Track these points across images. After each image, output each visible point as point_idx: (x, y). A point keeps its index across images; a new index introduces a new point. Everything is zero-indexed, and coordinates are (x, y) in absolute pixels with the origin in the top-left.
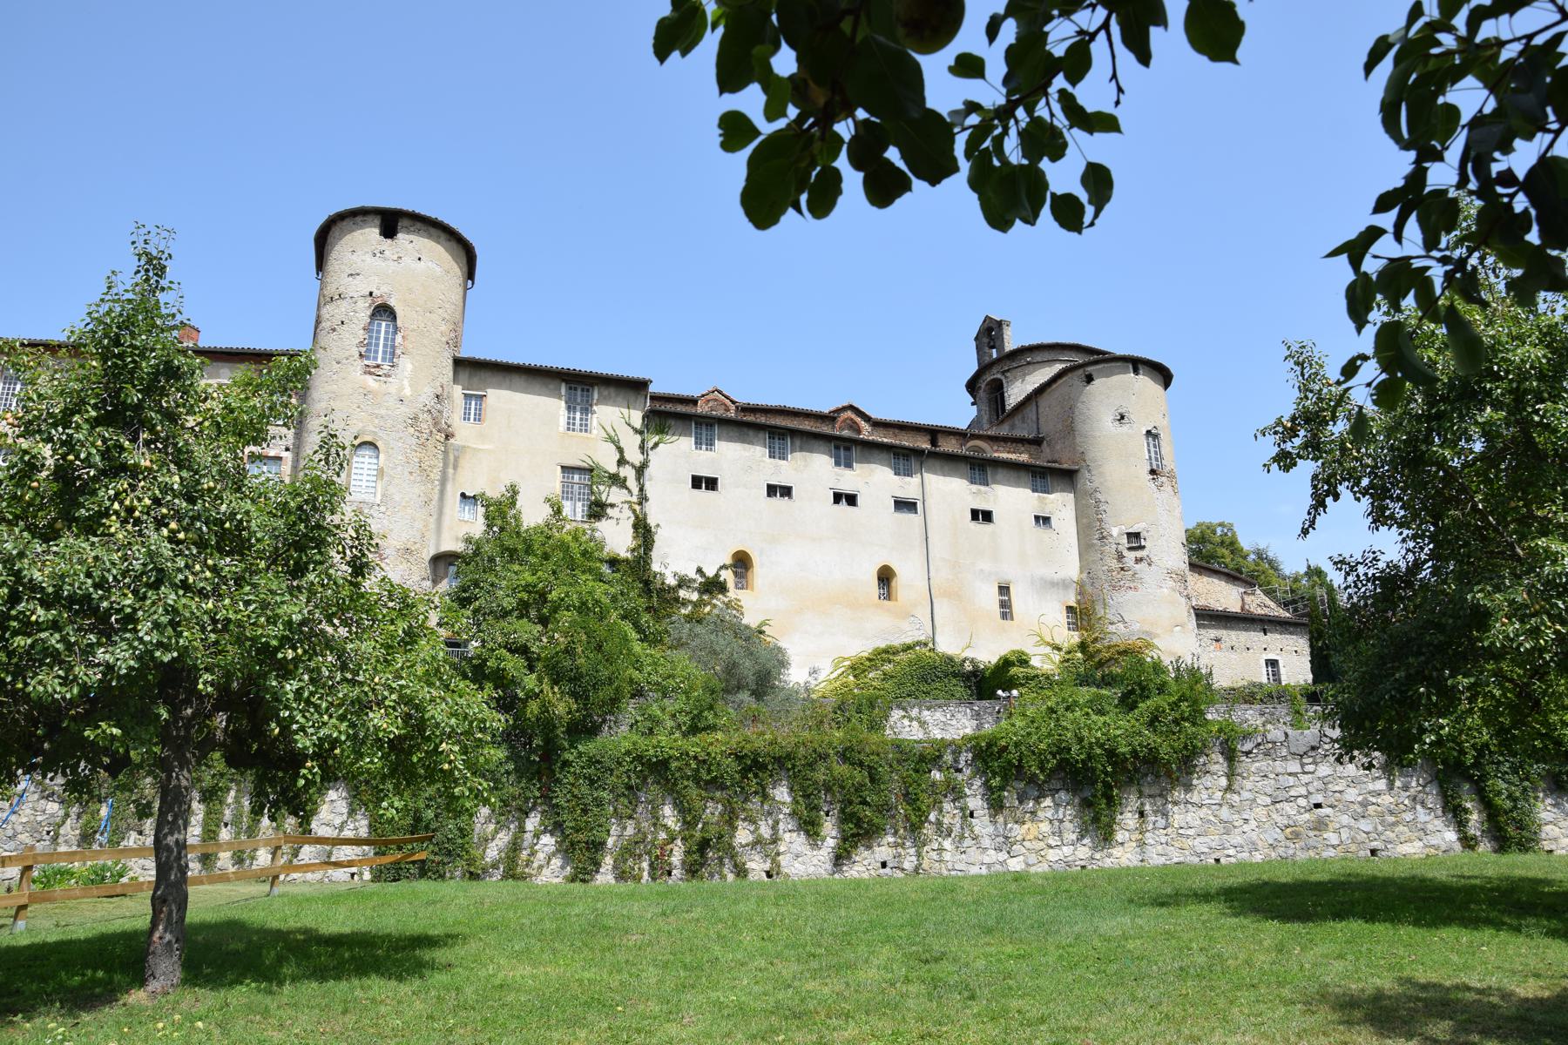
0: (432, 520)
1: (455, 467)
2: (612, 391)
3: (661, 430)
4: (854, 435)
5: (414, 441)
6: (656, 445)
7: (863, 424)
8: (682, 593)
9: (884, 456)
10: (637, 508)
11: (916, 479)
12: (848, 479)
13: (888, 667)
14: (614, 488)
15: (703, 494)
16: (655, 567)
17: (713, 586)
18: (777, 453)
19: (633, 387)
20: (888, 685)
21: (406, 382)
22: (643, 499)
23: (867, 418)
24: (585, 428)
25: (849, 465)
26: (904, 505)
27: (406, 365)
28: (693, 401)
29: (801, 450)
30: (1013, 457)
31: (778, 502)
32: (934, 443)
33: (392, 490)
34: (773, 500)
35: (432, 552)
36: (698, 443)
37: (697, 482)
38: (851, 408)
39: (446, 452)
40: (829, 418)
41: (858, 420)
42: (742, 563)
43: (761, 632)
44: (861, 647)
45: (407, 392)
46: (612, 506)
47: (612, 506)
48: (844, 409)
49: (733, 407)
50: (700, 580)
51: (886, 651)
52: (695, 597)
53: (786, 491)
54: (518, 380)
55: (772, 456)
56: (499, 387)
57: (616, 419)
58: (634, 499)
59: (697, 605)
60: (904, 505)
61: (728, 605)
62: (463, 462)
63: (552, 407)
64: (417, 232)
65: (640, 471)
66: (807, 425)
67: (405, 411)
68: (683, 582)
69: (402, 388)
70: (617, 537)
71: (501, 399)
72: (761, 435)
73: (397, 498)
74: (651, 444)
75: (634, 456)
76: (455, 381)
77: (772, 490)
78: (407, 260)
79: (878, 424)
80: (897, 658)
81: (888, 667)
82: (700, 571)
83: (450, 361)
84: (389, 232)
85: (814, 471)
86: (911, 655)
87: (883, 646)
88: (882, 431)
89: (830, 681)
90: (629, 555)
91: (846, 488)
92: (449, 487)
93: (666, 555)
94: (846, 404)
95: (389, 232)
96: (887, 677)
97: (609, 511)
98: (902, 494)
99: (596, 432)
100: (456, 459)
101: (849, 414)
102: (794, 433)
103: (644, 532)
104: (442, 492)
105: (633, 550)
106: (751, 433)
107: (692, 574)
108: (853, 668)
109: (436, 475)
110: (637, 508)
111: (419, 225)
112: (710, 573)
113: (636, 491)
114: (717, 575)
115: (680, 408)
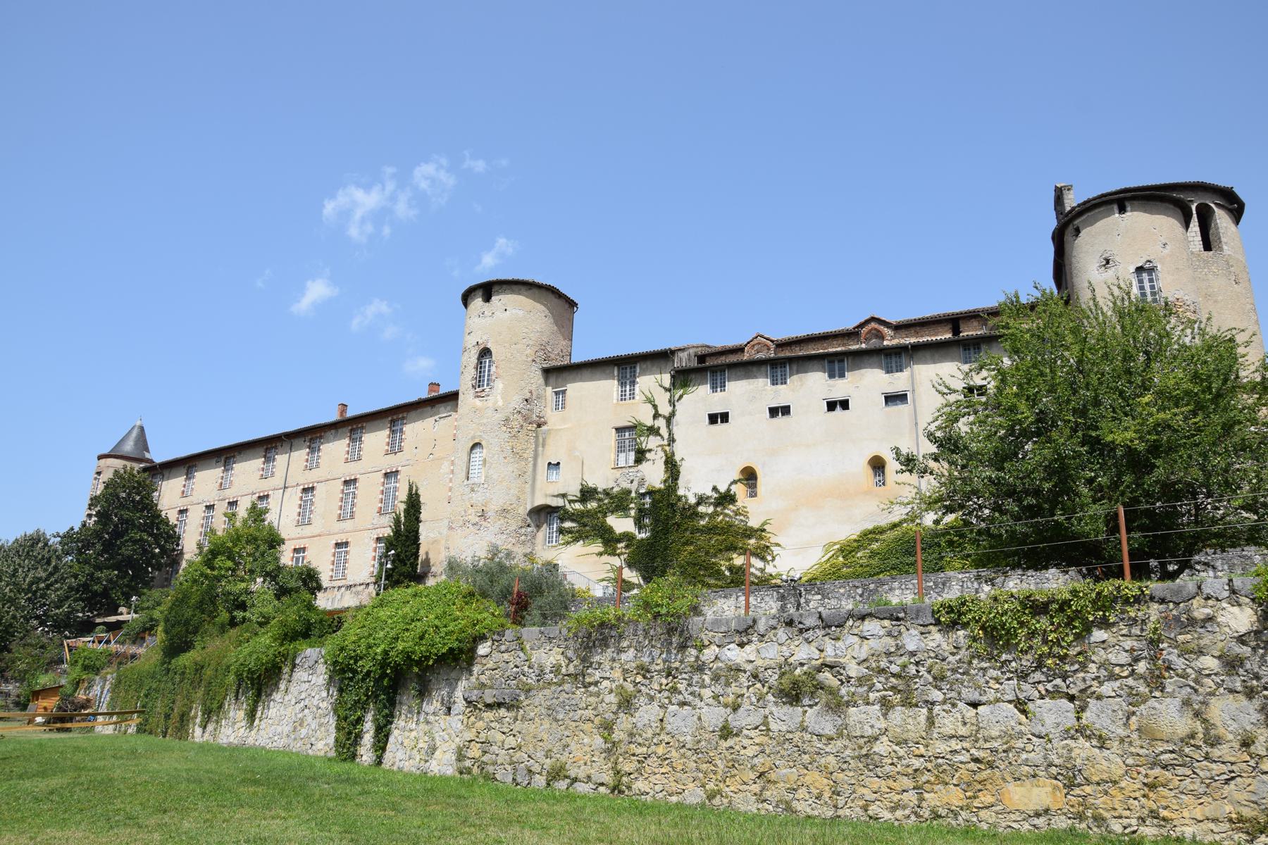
0: (528, 486)
1: (543, 446)
2: (649, 363)
3: (685, 385)
5: (507, 435)
6: (681, 397)
7: (885, 330)
8: (701, 509)
9: (875, 359)
10: (667, 448)
11: (906, 373)
12: (840, 388)
13: (875, 546)
14: (651, 437)
15: (720, 427)
16: (681, 492)
17: (726, 499)
18: (718, 386)
19: (660, 358)
20: (875, 562)
21: (499, 397)
22: (672, 440)
24: (632, 396)
25: (842, 375)
26: (894, 399)
27: (499, 385)
28: (740, 350)
29: (798, 372)
30: (913, 340)
31: (780, 420)
32: (956, 331)
33: (491, 472)
34: (714, 427)
35: (529, 508)
36: (714, 388)
37: (713, 419)
38: (873, 319)
39: (537, 437)
40: (852, 335)
41: (881, 328)
42: (749, 476)
43: (764, 530)
44: (848, 531)
45: (500, 403)
46: (650, 451)
47: (650, 451)
49: (773, 346)
50: (716, 495)
51: (871, 532)
52: (711, 510)
53: (786, 410)
54: (586, 373)
55: (774, 383)
56: (574, 381)
57: (652, 383)
58: (666, 442)
59: (712, 516)
60: (894, 399)
61: (737, 513)
62: (549, 441)
63: (609, 386)
64: (504, 292)
65: (669, 420)
67: (500, 416)
68: (701, 500)
69: (496, 402)
70: (654, 474)
71: (577, 389)
72: (763, 368)
73: (495, 477)
74: (677, 397)
75: (665, 409)
76: (547, 384)
77: (774, 412)
78: (498, 314)
80: (884, 537)
81: (875, 546)
82: (715, 489)
83: (539, 373)
84: (487, 299)
85: (812, 386)
86: (896, 533)
87: (870, 527)
88: (903, 333)
89: (821, 564)
90: (662, 486)
91: (838, 396)
92: (539, 460)
93: (688, 482)
94: (867, 317)
95: (487, 299)
96: (873, 554)
97: (648, 455)
98: (891, 390)
99: (639, 397)
100: (544, 440)
101: (873, 325)
102: (791, 360)
103: (672, 467)
104: (535, 465)
105: (665, 481)
106: (755, 369)
107: (709, 493)
108: (841, 550)
109: (529, 454)
110: (667, 448)
112: (723, 489)
113: (666, 436)
114: (729, 490)
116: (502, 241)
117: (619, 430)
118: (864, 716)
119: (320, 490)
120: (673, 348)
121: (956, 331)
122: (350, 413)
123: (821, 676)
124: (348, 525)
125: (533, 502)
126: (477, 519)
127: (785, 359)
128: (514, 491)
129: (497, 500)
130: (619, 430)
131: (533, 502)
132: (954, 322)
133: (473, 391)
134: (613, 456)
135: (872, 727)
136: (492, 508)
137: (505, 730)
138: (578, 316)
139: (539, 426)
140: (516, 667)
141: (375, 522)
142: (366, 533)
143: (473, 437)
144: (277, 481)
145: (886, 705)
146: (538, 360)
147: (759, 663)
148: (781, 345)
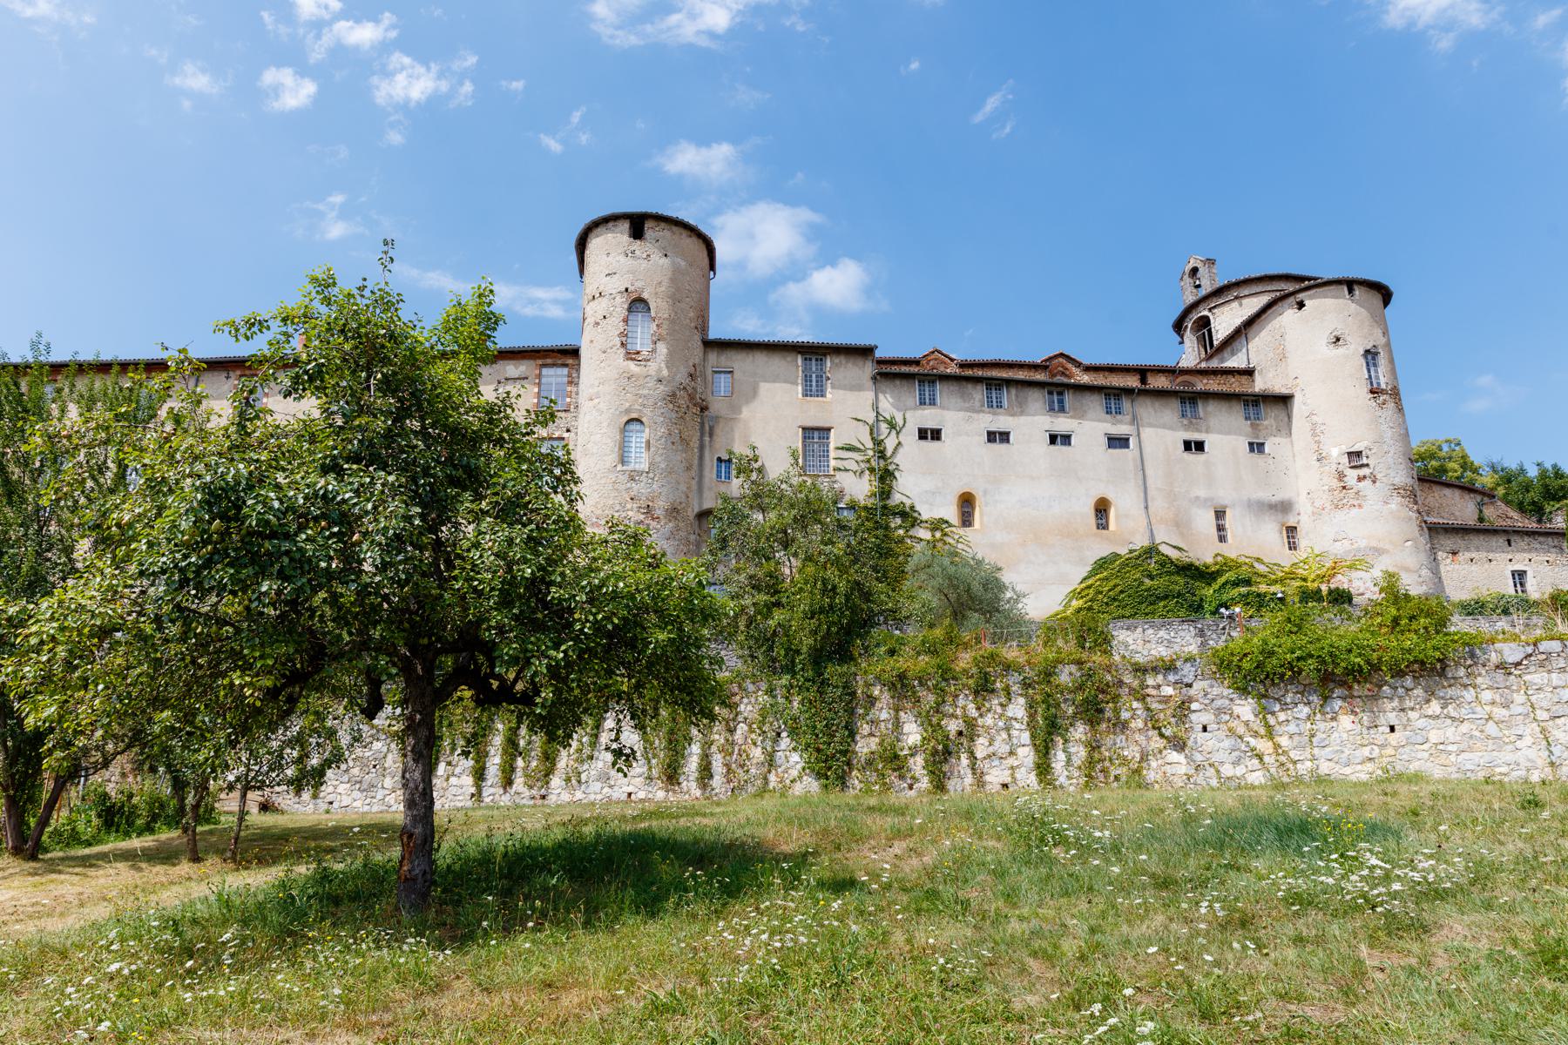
1: (711, 435)
4: (1065, 380)
19: (865, 352)
23: (1078, 364)
28: (917, 362)
32: (1143, 381)
34: (923, 443)
35: (696, 510)
38: (1062, 355)
39: (702, 424)
41: (1070, 366)
42: (967, 503)
48: (1056, 357)
66: (1021, 375)
79: (1089, 369)
91: (930, 424)
95: (637, 234)
100: (711, 428)
102: (1009, 382)
104: (701, 458)
109: (695, 443)
111: (663, 225)
115: (905, 369)
116: (800, 175)
121: (1143, 381)
125: (700, 504)
126: (642, 517)
127: (991, 379)
131: (700, 504)
132: (1143, 372)
143: (628, 411)
148: (963, 365)
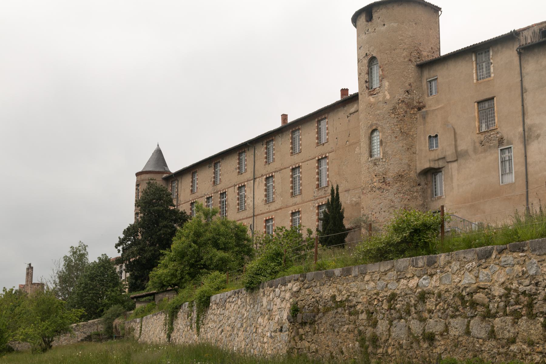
21: (386, 93)
69: (385, 96)
117: (479, 103)
118: (504, 324)
119: (277, 176)
120: (517, 29)
122: (290, 120)
123: (476, 296)
124: (298, 199)
128: (405, 161)
129: (393, 169)
130: (479, 103)
133: (367, 91)
134: (477, 124)
135: (509, 331)
136: (391, 175)
137: (310, 340)
138: (443, 19)
139: (419, 109)
140: (313, 297)
141: (315, 194)
142: (310, 204)
143: (371, 126)
144: (249, 175)
145: (516, 315)
146: (413, 59)
147: (442, 287)
